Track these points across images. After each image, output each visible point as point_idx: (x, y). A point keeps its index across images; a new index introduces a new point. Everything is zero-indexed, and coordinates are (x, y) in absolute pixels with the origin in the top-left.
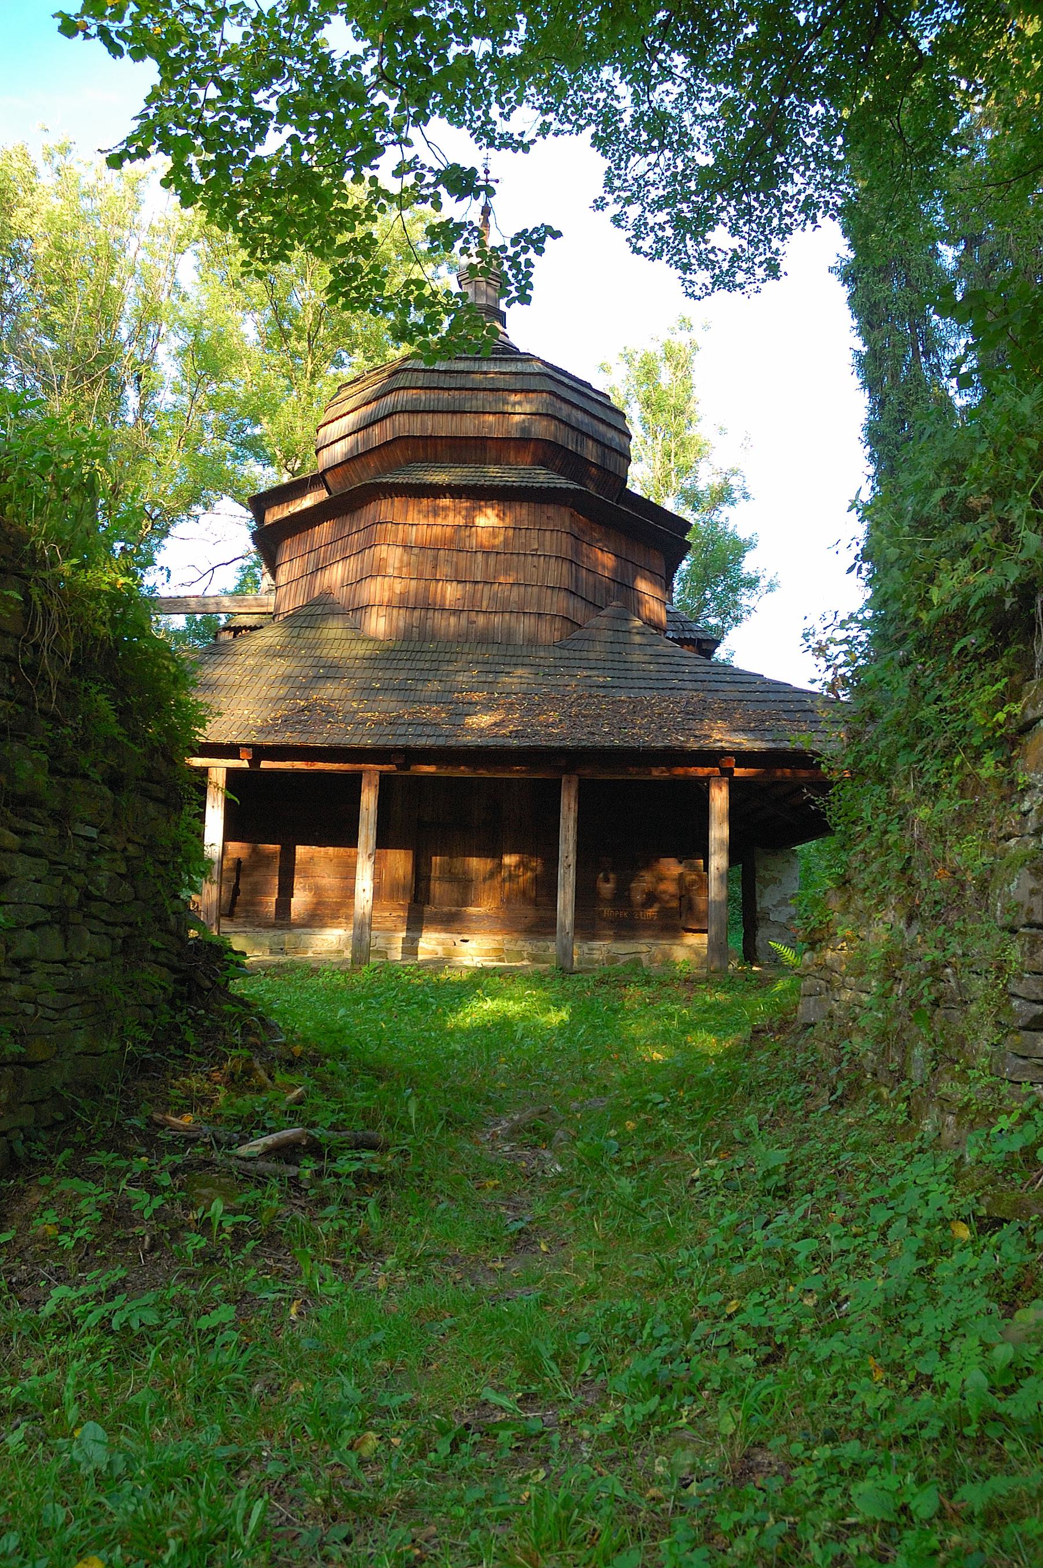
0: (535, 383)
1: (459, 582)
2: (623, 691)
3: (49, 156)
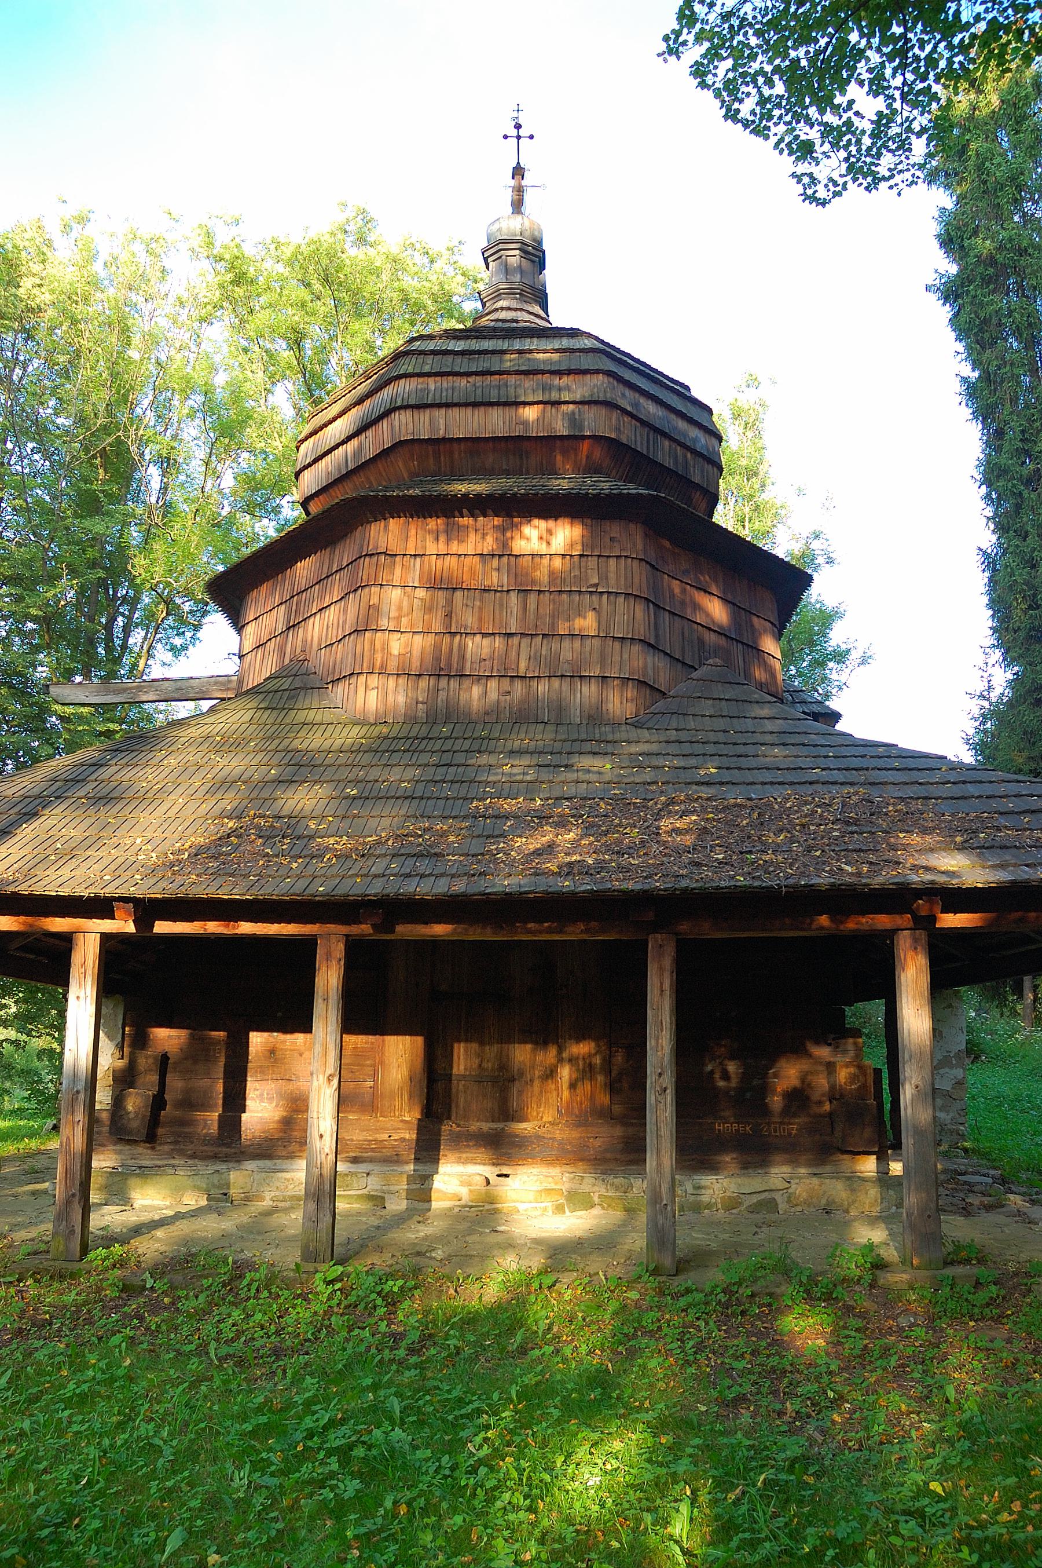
0: (587, 362)
1: (485, 635)
2: (738, 789)
3: (67, 229)
